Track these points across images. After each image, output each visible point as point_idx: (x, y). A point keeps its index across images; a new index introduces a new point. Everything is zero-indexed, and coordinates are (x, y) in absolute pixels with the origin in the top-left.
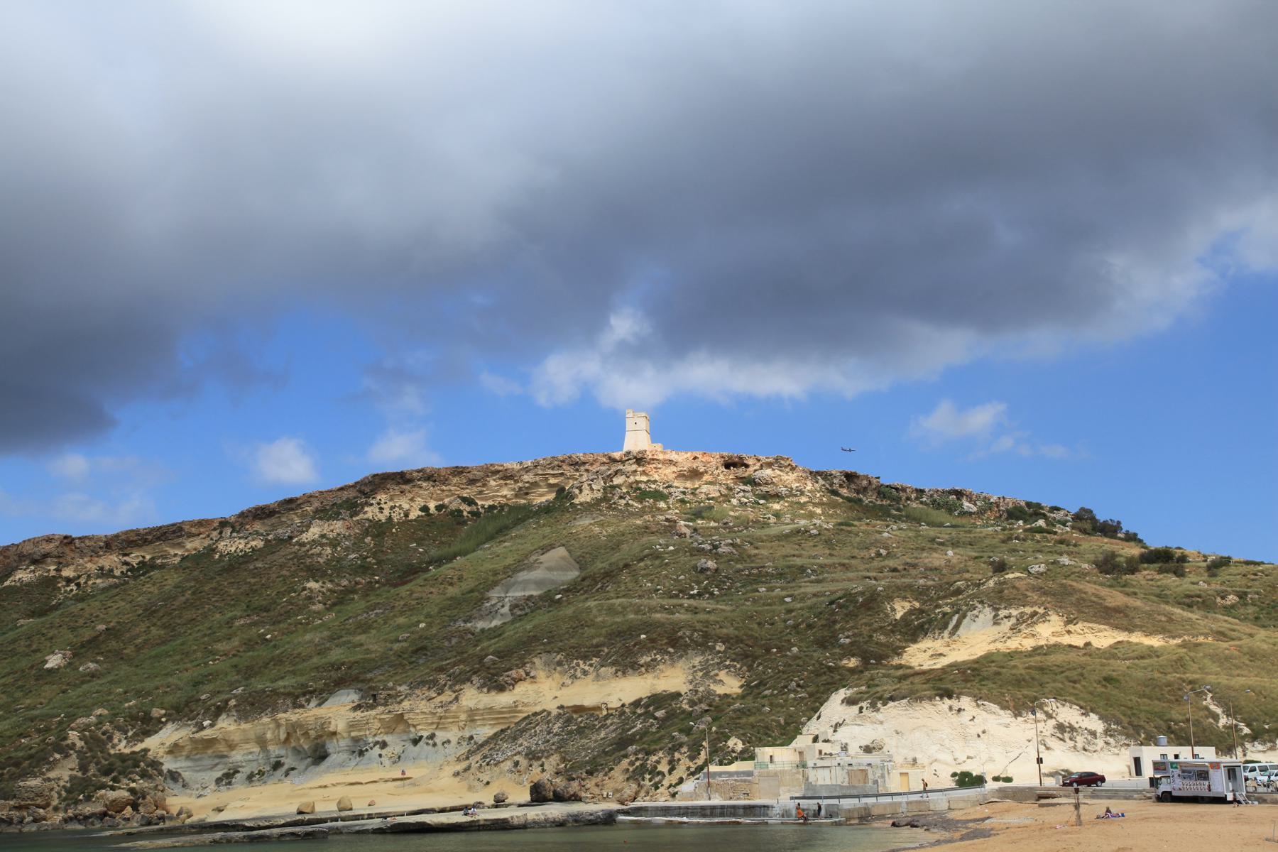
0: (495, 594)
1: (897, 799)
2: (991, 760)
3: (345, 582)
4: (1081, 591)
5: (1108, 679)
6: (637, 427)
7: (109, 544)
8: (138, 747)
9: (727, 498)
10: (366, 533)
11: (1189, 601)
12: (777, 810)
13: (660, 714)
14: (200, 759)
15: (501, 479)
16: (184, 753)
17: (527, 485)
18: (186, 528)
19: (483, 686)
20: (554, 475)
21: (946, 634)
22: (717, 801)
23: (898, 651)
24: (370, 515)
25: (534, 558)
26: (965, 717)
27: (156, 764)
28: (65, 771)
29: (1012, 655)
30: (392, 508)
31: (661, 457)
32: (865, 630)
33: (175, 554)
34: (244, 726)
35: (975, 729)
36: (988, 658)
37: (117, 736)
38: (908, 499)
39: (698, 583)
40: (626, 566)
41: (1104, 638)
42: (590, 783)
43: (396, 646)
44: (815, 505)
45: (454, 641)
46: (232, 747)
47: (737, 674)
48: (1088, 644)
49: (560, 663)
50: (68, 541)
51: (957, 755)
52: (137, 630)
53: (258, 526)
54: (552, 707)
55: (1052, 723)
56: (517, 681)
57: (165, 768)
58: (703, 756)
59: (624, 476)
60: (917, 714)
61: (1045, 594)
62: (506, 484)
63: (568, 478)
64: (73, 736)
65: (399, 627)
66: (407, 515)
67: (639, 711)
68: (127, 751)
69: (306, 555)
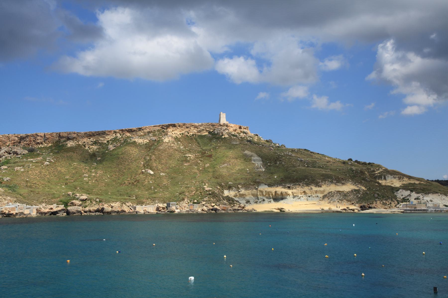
14: (240, 198)
15: (194, 127)
16: (238, 197)
17: (201, 130)
18: (107, 132)
20: (208, 128)
22: (408, 209)
60: (434, 196)
62: (195, 129)
63: (211, 129)
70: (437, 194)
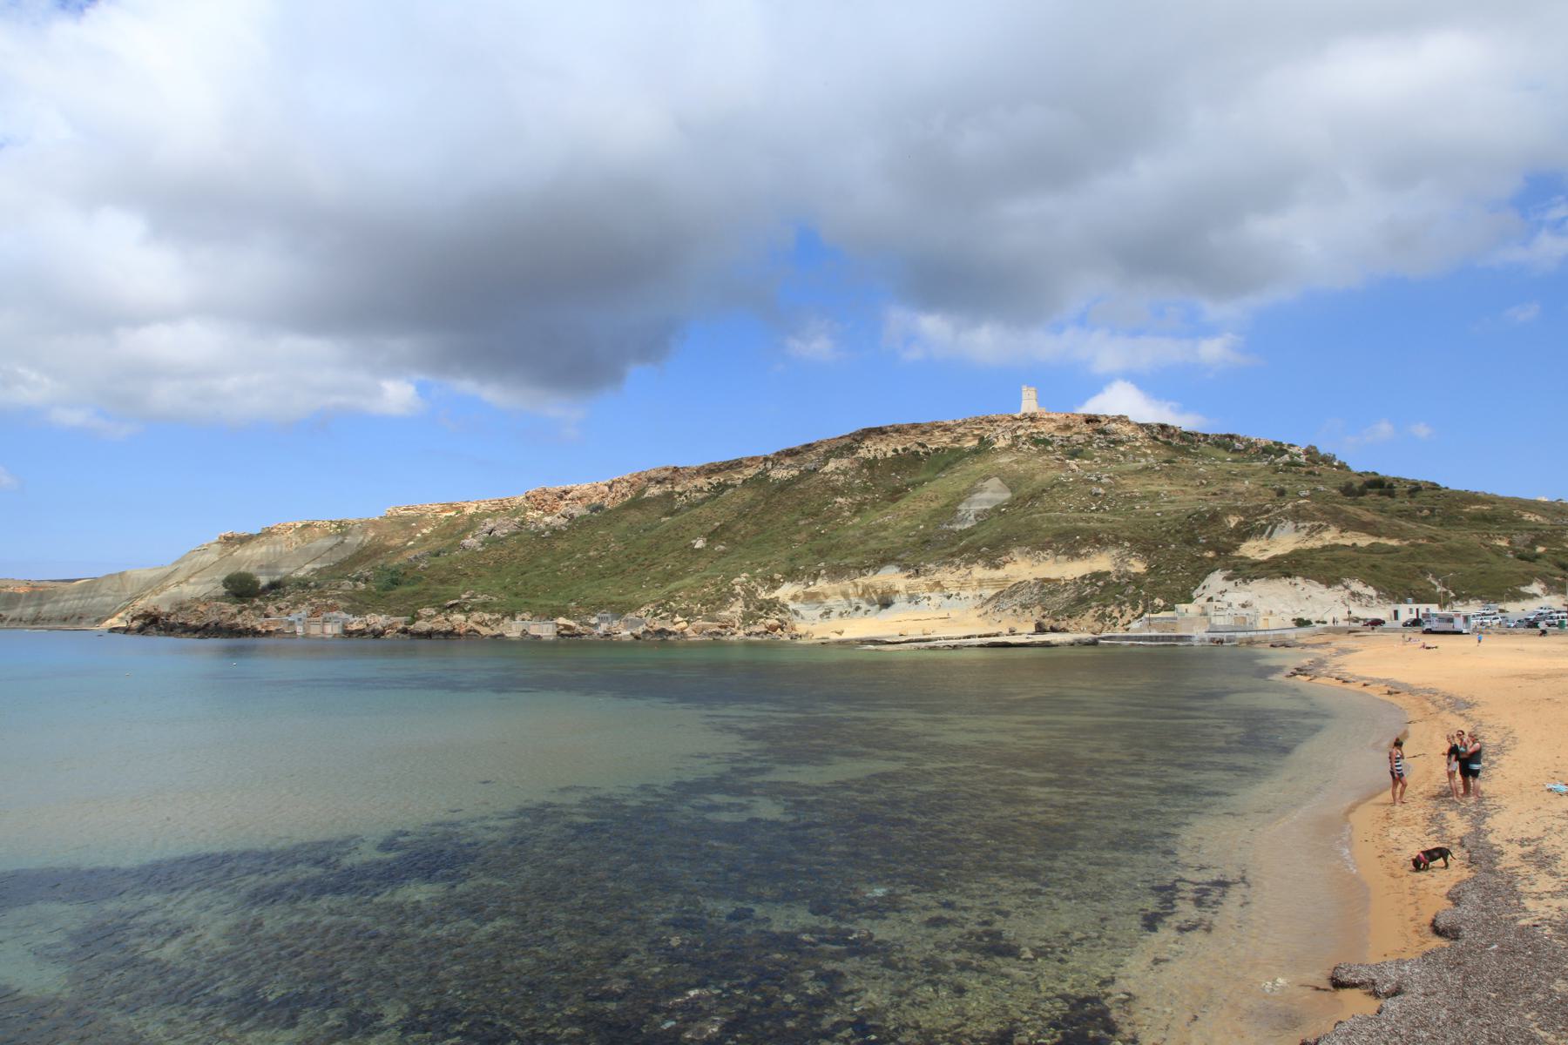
0: (963, 507)
1: (1268, 633)
2: (1314, 612)
3: (859, 498)
4: (1346, 512)
5: (1374, 566)
7: (699, 472)
8: (773, 596)
9: (1090, 443)
10: (862, 466)
11: (1402, 514)
12: (1196, 638)
13: (1100, 583)
19: (986, 565)
21: (1264, 537)
22: (1154, 633)
23: (1236, 548)
24: (862, 455)
25: (980, 484)
26: (1299, 588)
27: (785, 606)
28: (737, 608)
29: (1311, 551)
30: (876, 450)
32: (1214, 534)
33: (738, 478)
34: (832, 585)
35: (1304, 595)
36: (1296, 553)
37: (760, 589)
38: (1199, 441)
39: (1095, 503)
40: (1044, 491)
41: (1364, 541)
42: (1072, 622)
43: (910, 539)
44: (1145, 447)
45: (945, 537)
46: (826, 597)
47: (1142, 560)
48: (1354, 544)
49: (1028, 553)
50: (676, 470)
51: (1295, 609)
52: (739, 526)
53: (788, 461)
54: (1031, 578)
55: (1347, 592)
56: (1005, 563)
57: (791, 607)
58: (1140, 609)
61: (1325, 513)
64: (738, 588)
65: (906, 528)
66: (885, 455)
67: (1086, 582)
68: (767, 598)
69: (829, 481)
70: (1286, 581)
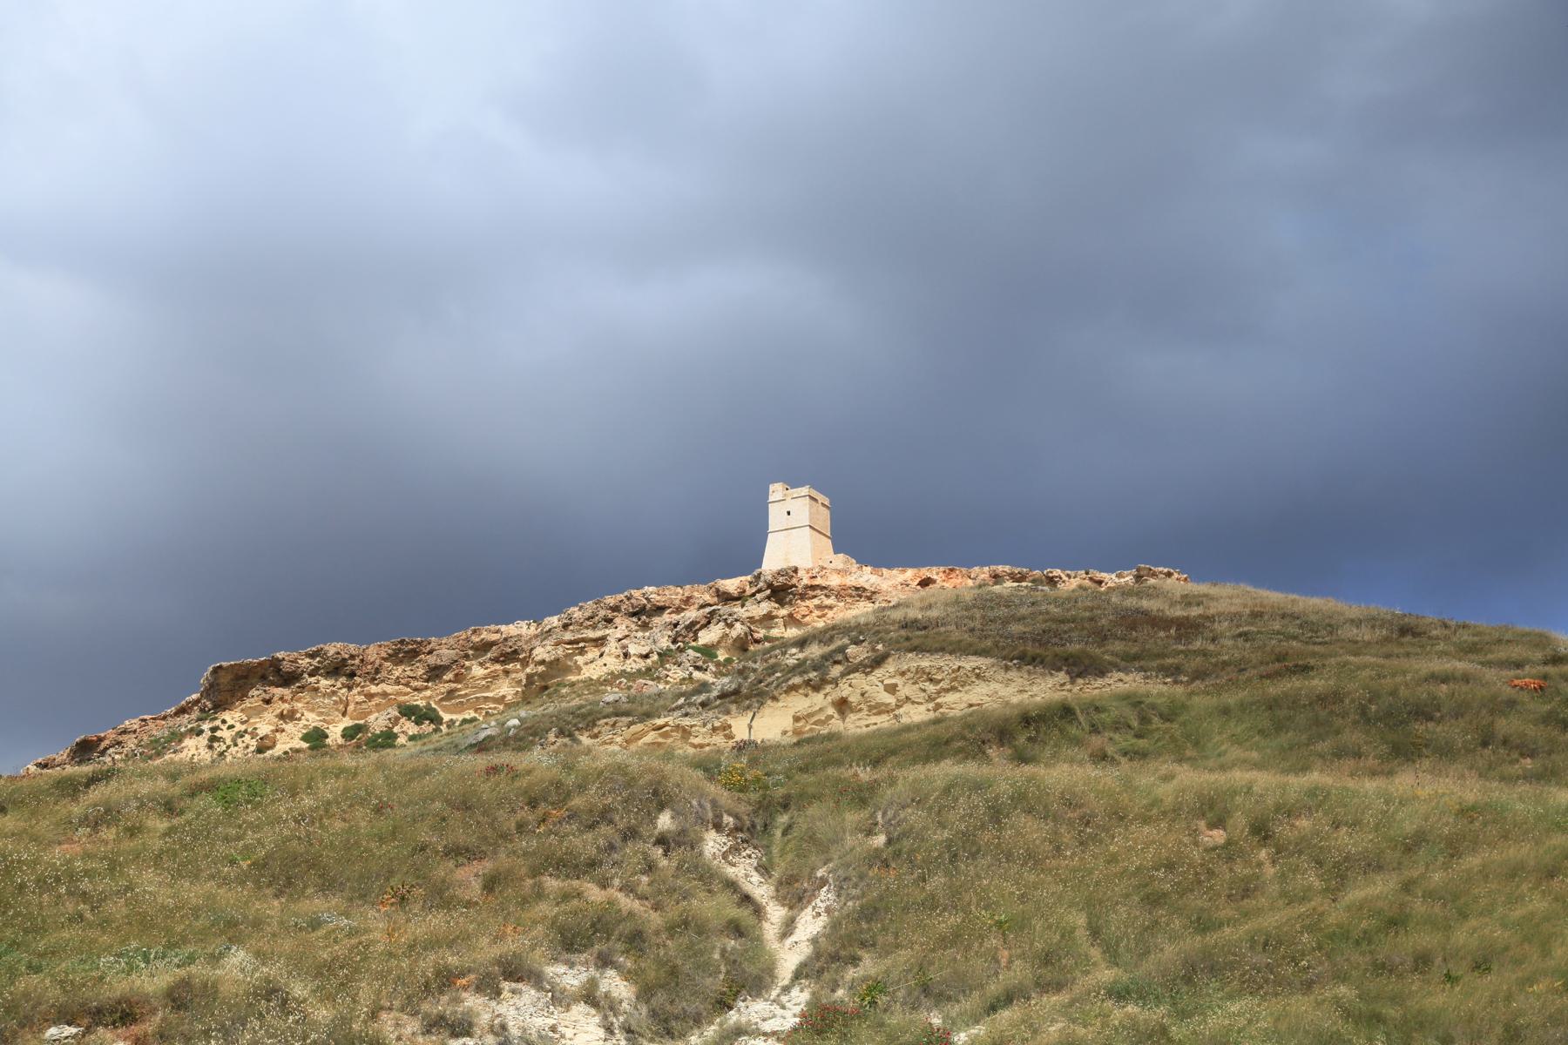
6: (793, 521)
15: (495, 660)
17: (541, 668)
31: (834, 581)
59: (722, 624)
62: (507, 672)
